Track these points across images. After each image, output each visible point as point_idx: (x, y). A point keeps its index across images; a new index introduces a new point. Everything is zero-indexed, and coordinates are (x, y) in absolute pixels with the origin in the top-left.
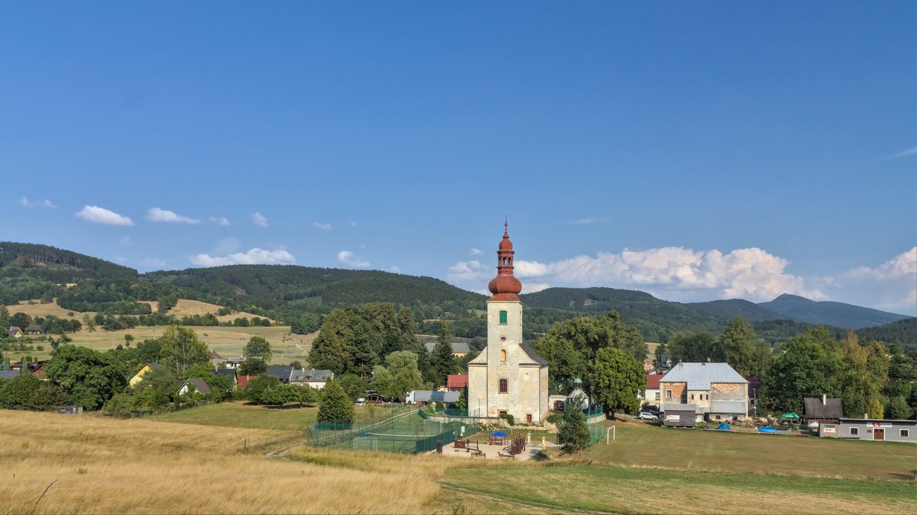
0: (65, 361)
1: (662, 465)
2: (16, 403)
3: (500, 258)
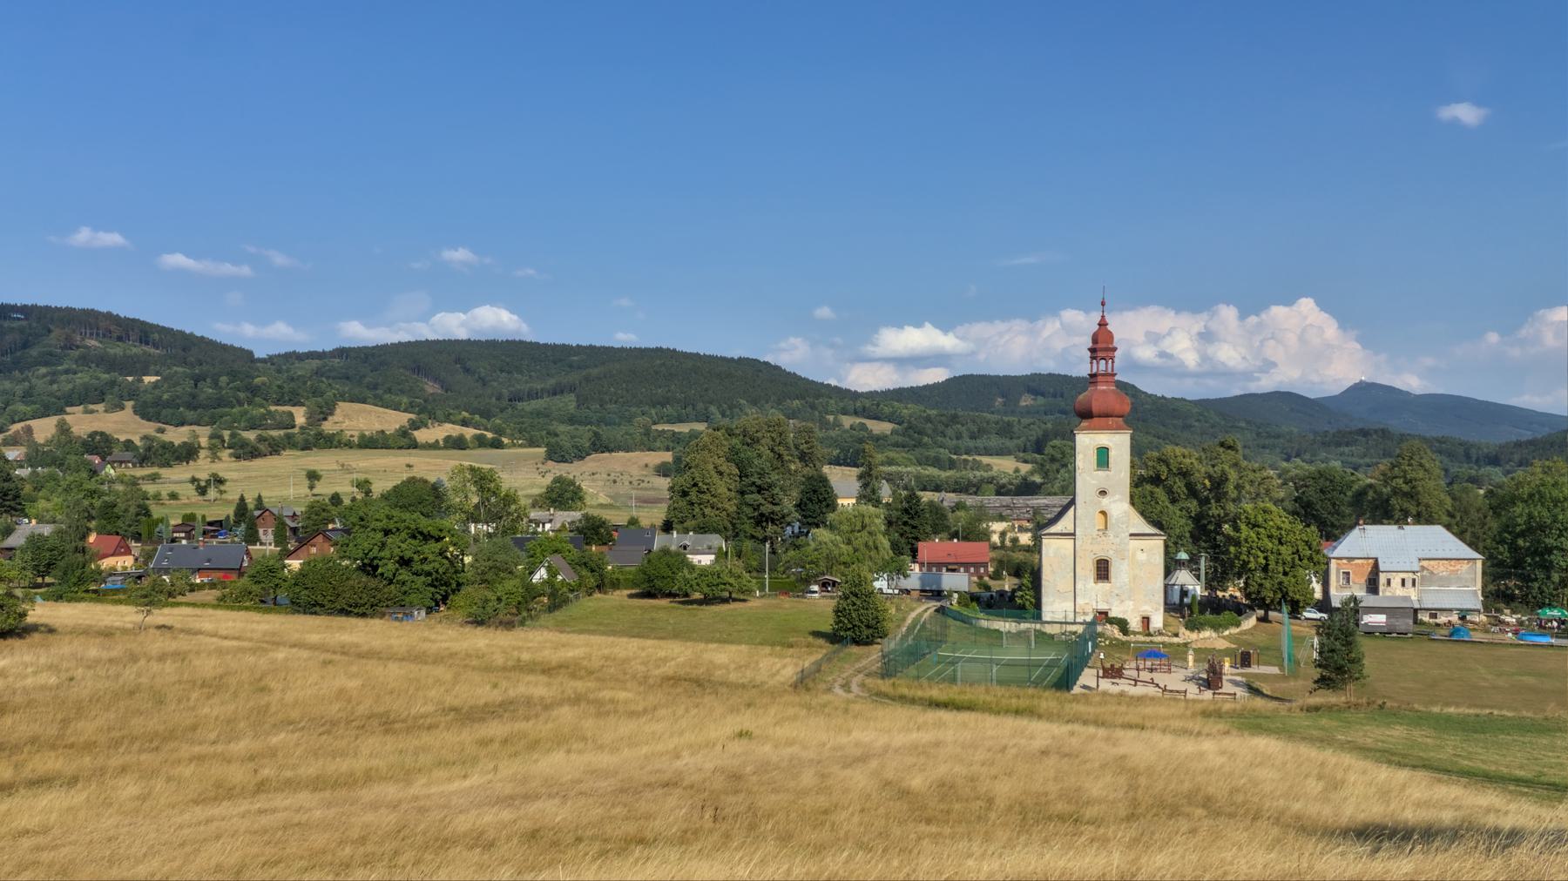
0: (380, 535)
1: (1457, 705)
2: (316, 604)
3: (1093, 358)
